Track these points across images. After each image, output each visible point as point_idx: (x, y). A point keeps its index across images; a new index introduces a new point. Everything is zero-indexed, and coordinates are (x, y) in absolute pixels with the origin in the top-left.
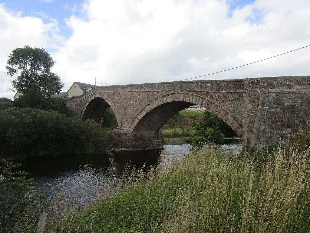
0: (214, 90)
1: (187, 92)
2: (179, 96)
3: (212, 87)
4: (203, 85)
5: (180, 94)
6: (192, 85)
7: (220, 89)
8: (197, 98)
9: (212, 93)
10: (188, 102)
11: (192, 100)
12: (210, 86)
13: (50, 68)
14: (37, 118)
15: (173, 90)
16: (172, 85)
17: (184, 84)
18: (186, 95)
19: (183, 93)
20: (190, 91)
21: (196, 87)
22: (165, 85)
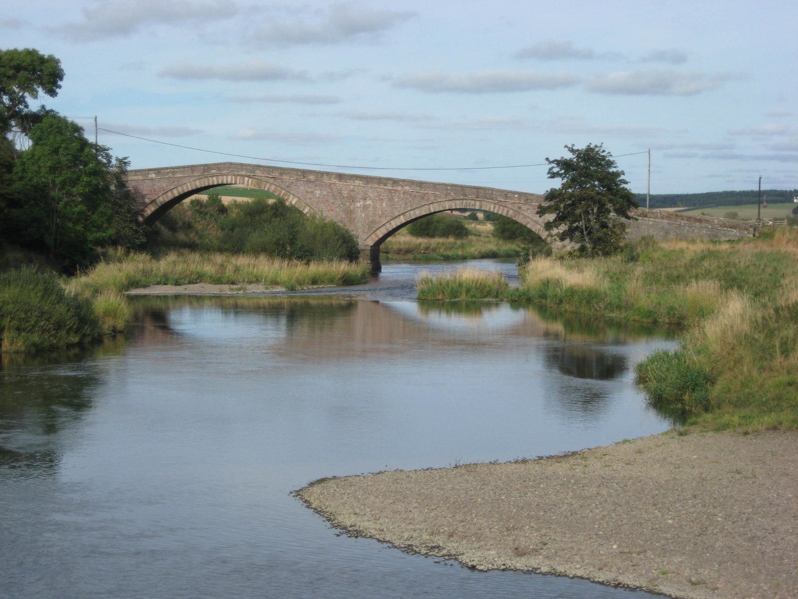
0: (522, 201)
1: (485, 200)
2: (473, 202)
3: (519, 198)
4: (508, 195)
5: (476, 200)
6: (494, 193)
7: (529, 201)
8: (238, 178)
9: (520, 205)
10: (504, 215)
11: (248, 182)
12: (517, 198)
13: (90, 142)
14: (111, 262)
15: (463, 195)
16: (462, 190)
17: (481, 191)
18: (484, 203)
19: (480, 201)
20: (490, 199)
21: (499, 196)
22: (239, 167)
